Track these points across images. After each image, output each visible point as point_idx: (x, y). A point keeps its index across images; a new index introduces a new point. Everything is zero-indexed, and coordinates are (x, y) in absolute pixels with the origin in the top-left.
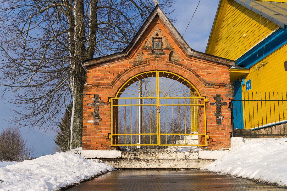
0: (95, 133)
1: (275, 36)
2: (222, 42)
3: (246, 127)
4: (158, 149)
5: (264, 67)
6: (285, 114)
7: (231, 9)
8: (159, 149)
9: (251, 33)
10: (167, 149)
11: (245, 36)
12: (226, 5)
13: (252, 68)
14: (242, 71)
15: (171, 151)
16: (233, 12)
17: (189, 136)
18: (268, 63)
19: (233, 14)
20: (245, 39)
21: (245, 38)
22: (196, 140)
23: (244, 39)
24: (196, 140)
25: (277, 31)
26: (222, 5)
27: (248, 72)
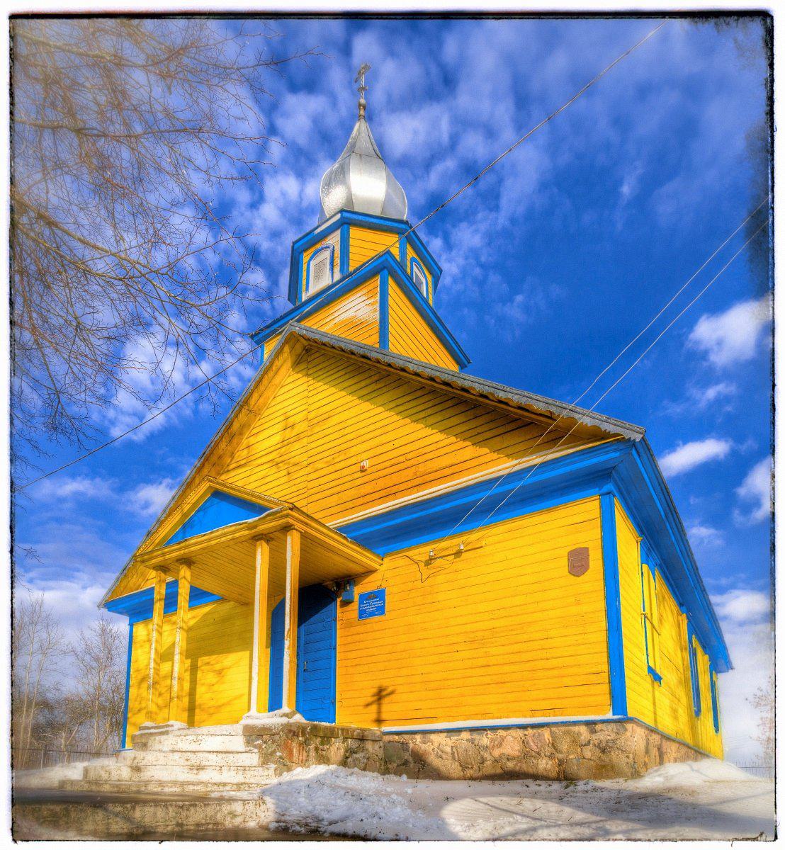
0: (156, 714)
1: (572, 463)
2: (248, 473)
3: (759, 749)
4: (188, 810)
5: (457, 560)
6: (242, 695)
7: (301, 388)
8: (192, 809)
9: (402, 459)
10: (229, 807)
11: (366, 464)
12: (283, 371)
13: (396, 556)
14: (365, 558)
15: (249, 813)
16: (310, 394)
17: (187, 737)
18: (482, 547)
19: (311, 400)
20: (363, 474)
21: (367, 473)
22: (225, 752)
23: (359, 474)
24: (225, 752)
25: (591, 450)
26: (275, 364)
27: (376, 566)
